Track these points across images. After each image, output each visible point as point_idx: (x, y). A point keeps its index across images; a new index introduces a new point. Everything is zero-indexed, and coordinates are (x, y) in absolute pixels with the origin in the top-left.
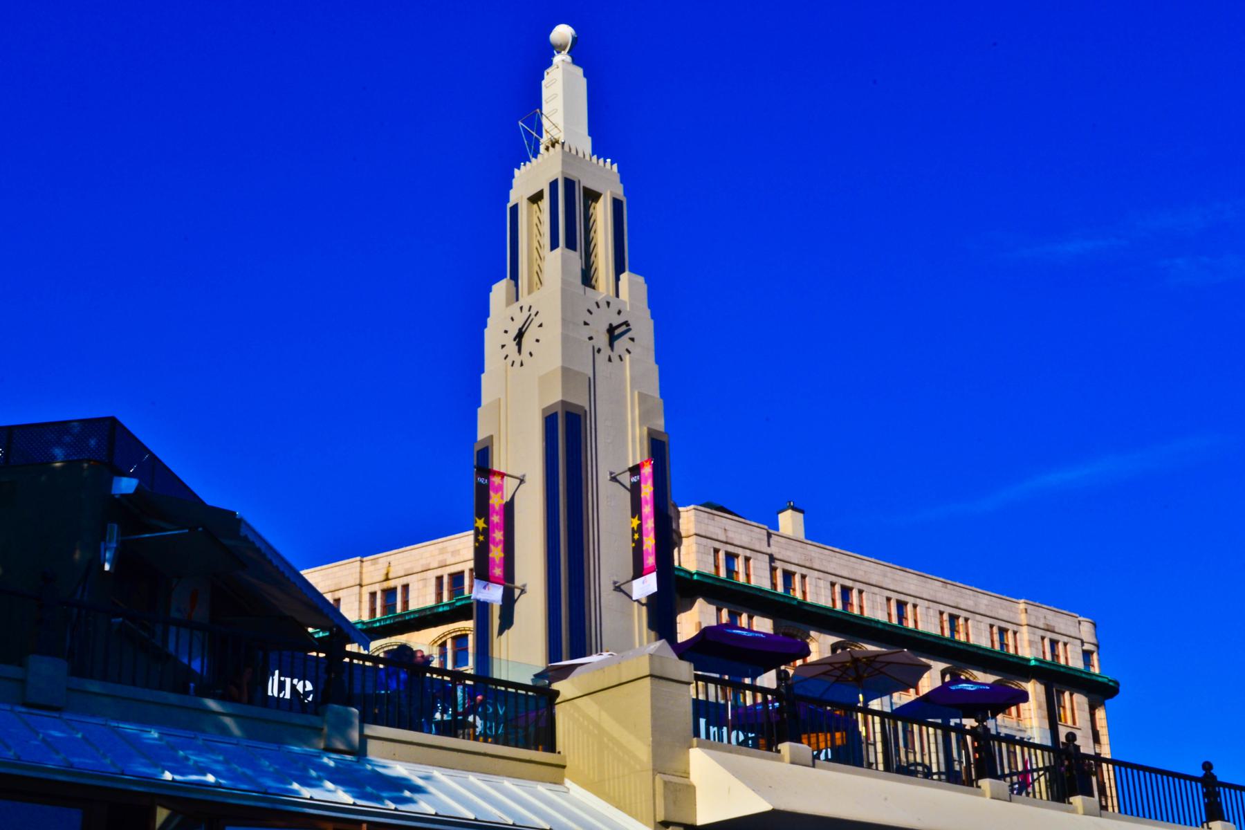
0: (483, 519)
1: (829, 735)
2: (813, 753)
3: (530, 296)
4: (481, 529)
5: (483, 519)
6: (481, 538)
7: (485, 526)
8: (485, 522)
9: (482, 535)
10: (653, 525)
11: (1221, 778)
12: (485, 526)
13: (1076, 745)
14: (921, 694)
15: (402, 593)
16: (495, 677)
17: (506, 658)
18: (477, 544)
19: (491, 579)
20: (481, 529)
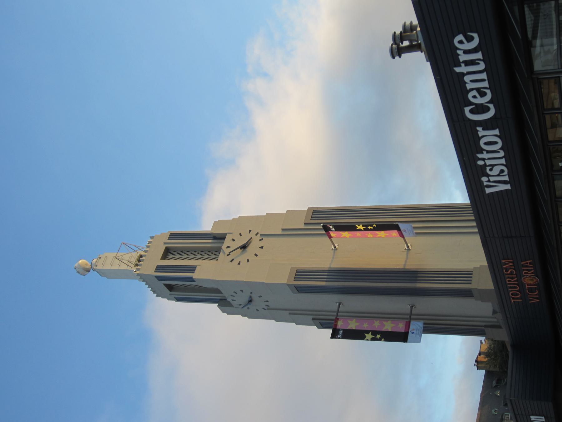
0: (366, 335)
1: (471, 206)
2: (395, 237)
3: (394, 32)
4: (372, 336)
5: (366, 335)
6: (378, 336)
7: (370, 333)
8: (368, 333)
9: (377, 336)
10: (347, 232)
11: (134, 265)
12: (370, 333)
13: (144, 282)
14: (486, 78)
15: (535, 297)
16: (307, 209)
17: (488, 164)
18: (383, 340)
19: (407, 331)
20: (372, 336)
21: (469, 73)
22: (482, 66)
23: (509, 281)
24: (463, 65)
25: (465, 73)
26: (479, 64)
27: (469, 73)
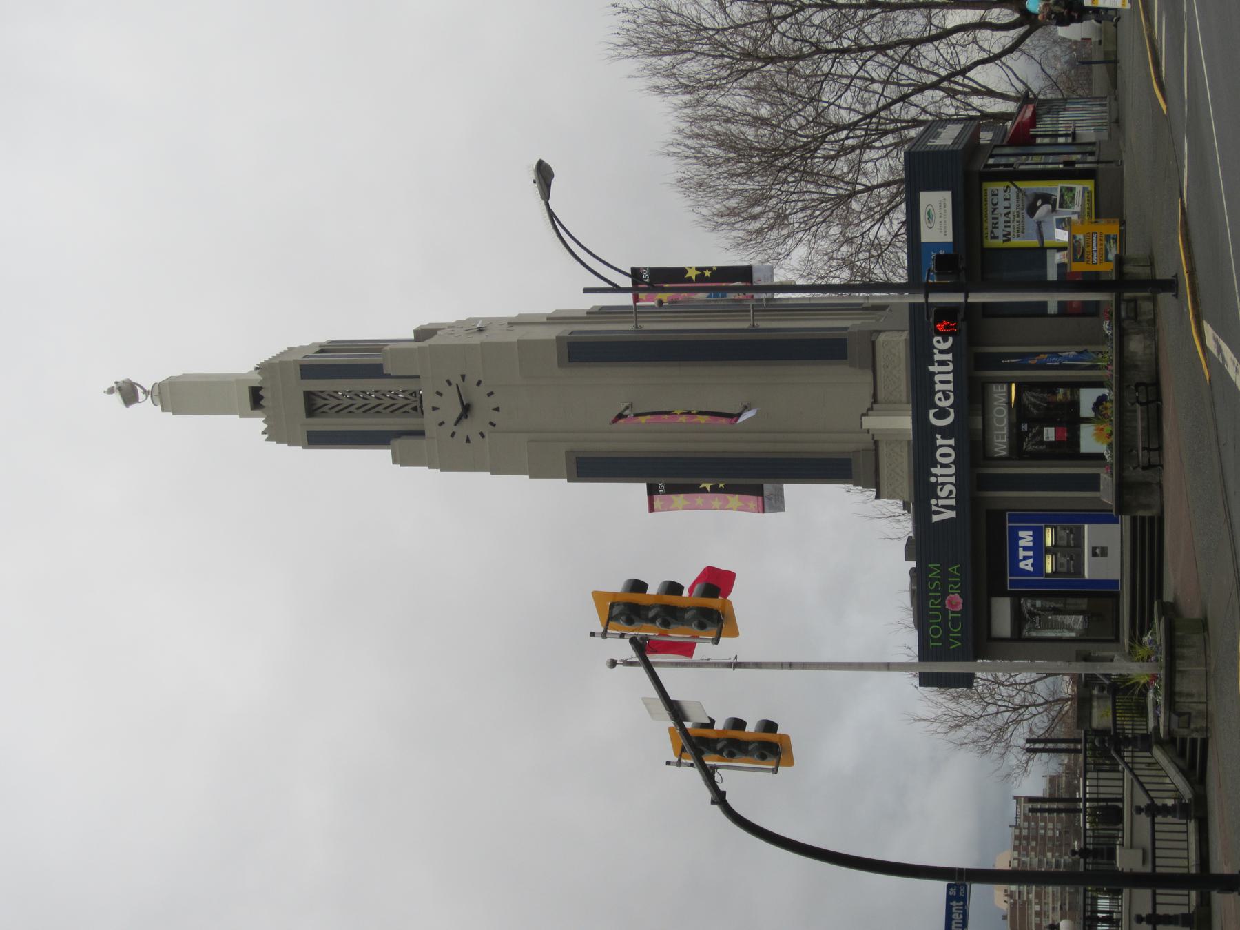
21: (939, 373)
22: (950, 368)
23: (932, 604)
24: (936, 364)
25: (936, 372)
26: (948, 365)
27: (939, 373)
